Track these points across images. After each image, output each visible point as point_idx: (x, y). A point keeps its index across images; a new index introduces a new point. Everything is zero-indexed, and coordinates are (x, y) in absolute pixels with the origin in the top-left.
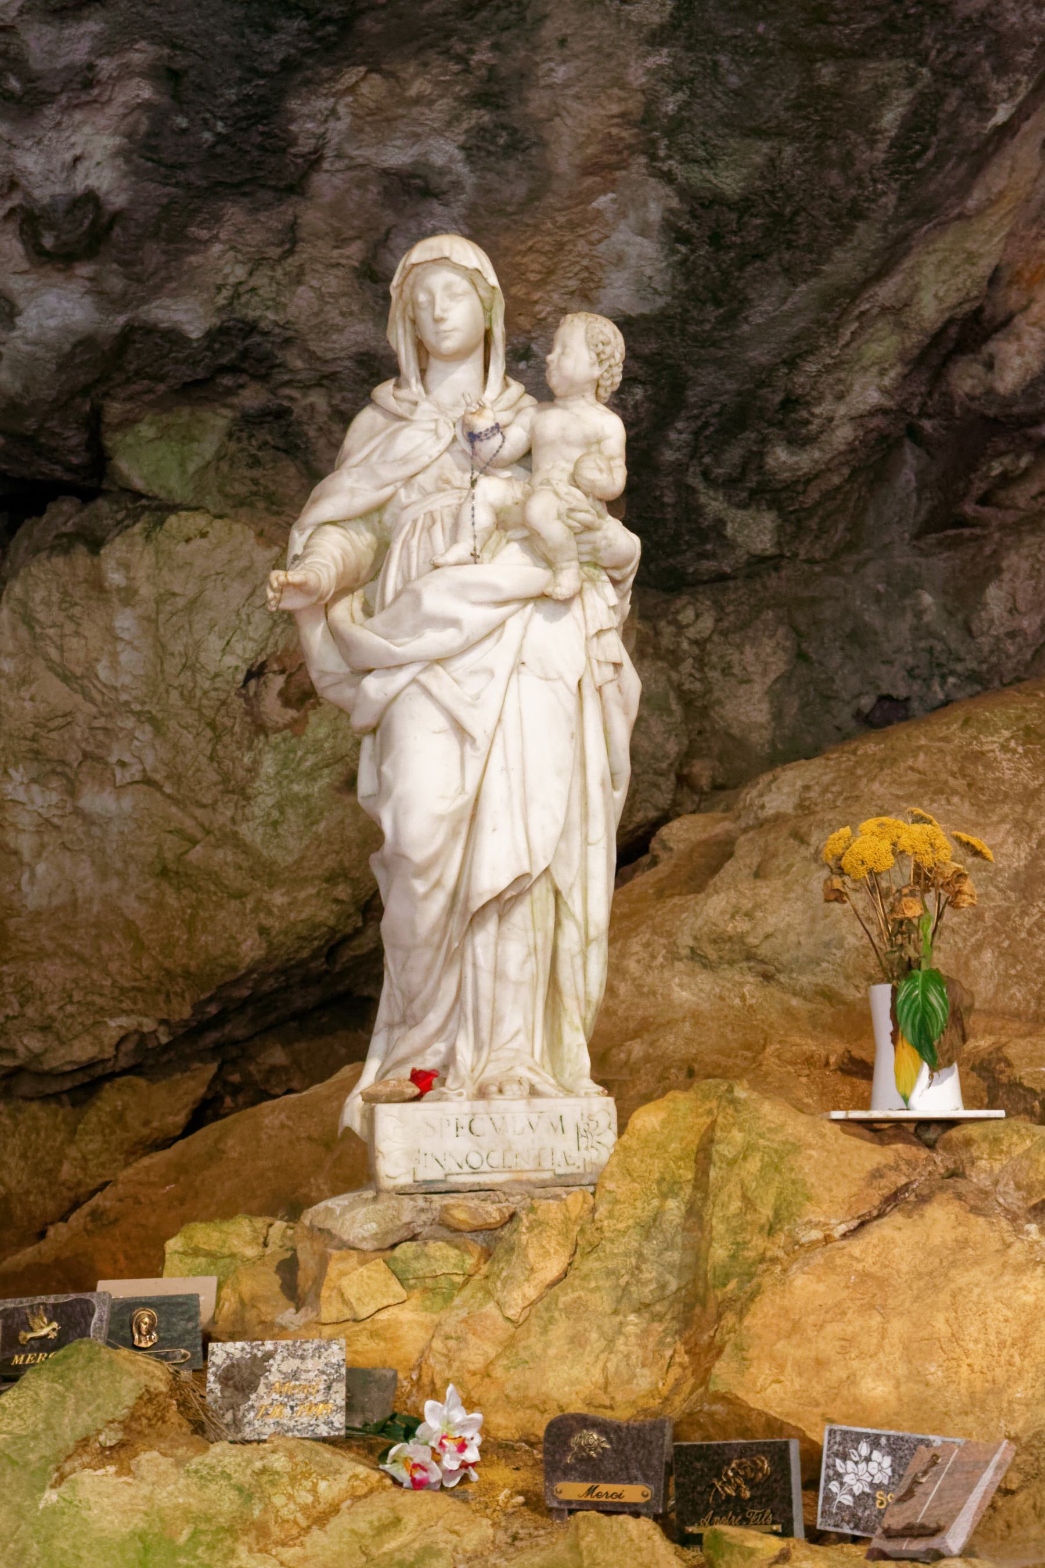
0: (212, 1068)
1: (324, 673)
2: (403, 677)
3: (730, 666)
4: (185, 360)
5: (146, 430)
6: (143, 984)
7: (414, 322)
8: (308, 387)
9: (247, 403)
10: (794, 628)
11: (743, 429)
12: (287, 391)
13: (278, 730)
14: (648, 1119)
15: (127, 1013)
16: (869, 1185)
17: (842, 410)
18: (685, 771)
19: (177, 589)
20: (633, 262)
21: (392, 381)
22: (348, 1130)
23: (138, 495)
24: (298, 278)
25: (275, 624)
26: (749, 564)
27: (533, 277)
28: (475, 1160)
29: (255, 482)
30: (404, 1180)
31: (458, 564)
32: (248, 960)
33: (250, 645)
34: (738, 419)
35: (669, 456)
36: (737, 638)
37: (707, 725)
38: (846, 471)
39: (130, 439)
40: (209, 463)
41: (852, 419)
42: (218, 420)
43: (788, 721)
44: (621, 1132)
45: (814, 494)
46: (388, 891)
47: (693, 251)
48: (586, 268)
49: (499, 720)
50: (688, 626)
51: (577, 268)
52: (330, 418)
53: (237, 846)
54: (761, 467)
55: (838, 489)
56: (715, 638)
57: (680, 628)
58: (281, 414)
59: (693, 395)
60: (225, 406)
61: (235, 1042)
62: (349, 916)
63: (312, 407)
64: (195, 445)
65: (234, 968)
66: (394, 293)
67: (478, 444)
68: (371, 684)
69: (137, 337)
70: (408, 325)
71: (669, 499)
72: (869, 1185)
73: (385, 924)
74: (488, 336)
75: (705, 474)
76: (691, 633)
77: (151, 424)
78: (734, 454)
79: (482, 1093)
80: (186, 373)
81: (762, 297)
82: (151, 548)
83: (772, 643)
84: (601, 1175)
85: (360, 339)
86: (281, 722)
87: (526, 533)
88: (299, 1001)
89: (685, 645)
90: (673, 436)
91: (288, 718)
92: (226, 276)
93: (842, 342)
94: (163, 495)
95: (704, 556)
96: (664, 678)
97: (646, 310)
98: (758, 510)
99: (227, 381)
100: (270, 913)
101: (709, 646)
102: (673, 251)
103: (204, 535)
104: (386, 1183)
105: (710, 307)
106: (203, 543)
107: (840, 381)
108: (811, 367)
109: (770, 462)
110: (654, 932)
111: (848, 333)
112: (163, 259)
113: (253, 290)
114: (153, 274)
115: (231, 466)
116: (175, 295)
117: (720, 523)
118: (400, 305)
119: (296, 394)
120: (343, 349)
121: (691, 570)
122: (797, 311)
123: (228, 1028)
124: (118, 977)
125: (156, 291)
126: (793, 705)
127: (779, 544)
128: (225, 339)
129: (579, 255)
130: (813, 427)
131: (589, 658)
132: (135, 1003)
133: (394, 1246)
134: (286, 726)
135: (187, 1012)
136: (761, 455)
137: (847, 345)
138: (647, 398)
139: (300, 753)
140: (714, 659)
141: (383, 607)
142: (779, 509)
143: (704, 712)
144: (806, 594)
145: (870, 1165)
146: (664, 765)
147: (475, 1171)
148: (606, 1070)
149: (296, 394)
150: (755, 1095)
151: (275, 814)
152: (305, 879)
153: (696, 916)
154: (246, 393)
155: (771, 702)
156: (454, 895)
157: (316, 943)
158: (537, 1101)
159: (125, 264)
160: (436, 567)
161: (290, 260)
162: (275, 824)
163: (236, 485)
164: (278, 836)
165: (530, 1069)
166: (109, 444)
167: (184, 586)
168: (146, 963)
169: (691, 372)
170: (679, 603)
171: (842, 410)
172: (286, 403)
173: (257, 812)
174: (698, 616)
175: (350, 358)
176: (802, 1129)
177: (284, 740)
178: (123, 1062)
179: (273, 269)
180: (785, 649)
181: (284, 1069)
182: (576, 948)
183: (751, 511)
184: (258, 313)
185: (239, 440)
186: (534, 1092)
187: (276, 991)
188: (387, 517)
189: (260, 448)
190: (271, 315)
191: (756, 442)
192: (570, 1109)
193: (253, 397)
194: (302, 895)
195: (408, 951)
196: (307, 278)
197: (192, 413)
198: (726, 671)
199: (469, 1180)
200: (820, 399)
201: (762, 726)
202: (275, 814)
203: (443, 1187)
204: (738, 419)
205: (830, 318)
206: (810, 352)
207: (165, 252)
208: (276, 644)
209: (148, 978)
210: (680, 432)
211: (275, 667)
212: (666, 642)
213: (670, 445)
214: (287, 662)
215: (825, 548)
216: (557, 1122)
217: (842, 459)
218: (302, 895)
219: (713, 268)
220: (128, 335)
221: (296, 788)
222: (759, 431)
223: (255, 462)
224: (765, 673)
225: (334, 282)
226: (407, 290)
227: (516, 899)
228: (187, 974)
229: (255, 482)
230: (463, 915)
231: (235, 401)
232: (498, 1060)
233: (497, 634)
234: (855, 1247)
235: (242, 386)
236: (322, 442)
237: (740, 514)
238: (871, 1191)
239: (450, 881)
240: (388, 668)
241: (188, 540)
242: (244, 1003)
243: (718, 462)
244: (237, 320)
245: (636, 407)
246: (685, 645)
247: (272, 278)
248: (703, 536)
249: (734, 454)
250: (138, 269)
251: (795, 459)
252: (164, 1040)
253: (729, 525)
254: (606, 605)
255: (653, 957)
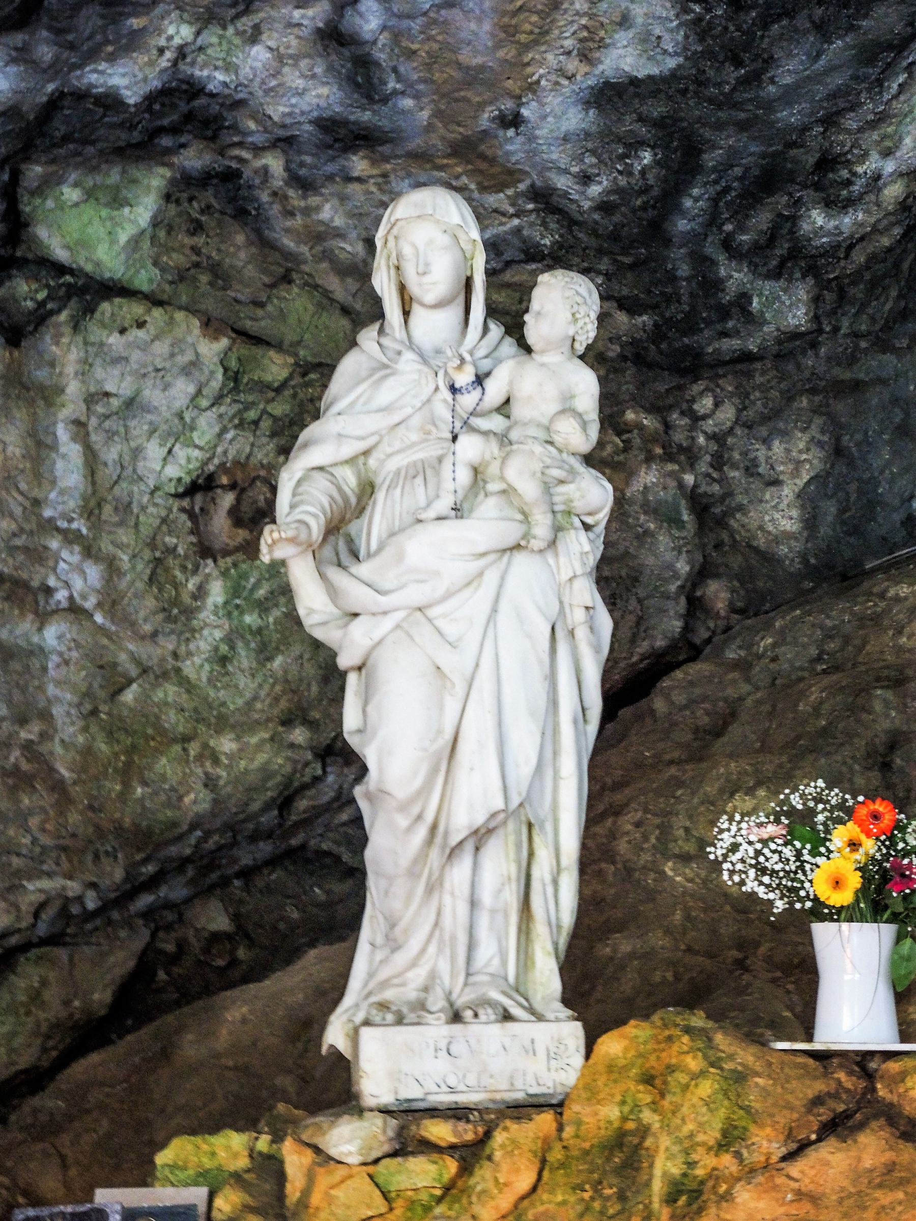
0: (144, 935)
1: (311, 611)
2: (387, 624)
3: (755, 463)
4: (121, 125)
5: (71, 194)
6: (67, 842)
7: (398, 268)
8: (264, 149)
9: (187, 163)
10: (832, 418)
11: (771, 192)
12: (236, 152)
13: (226, 553)
14: (612, 1045)
15: (50, 875)
16: (809, 1111)
17: (889, 167)
18: (698, 593)
19: (110, 387)
20: (640, 20)
21: (377, 326)
22: (333, 1050)
23: (60, 269)
24: (254, 37)
25: (224, 430)
26: (779, 342)
27: (523, 38)
28: (452, 1081)
29: (196, 250)
30: (387, 1099)
31: (440, 518)
32: (191, 814)
33: (196, 453)
34: (768, 180)
35: (682, 225)
36: (763, 431)
37: (725, 536)
38: (897, 231)
39: (50, 203)
40: (143, 232)
41: (901, 175)
42: (155, 180)
43: (824, 531)
44: (588, 1056)
45: (859, 257)
46: (372, 826)
47: (709, 10)
48: (585, 27)
49: (477, 665)
50: (704, 417)
51: (575, 27)
52: (287, 184)
53: (180, 684)
54: (792, 232)
55: (889, 250)
56: (738, 431)
57: (696, 419)
58: (230, 176)
59: (711, 159)
60: (164, 164)
61: (169, 905)
62: (307, 764)
63: (266, 169)
64: (127, 210)
65: (175, 824)
66: (379, 243)
67: (458, 396)
68: (357, 629)
69: (66, 103)
70: (393, 271)
71: (684, 270)
72: (809, 1111)
73: (369, 854)
74: (468, 284)
75: (727, 244)
76: (709, 425)
77: (76, 185)
78: (762, 220)
79: (456, 1017)
80: (123, 137)
81: (790, 55)
82: (79, 339)
83: (806, 437)
84: (567, 1095)
85: (323, 104)
86: (232, 544)
87: (503, 486)
88: (245, 858)
89: (701, 440)
90: (688, 203)
91: (239, 539)
92: (170, 38)
93: (886, 97)
94: (89, 268)
95: (725, 334)
96: (673, 484)
97: (655, 71)
98: (790, 280)
99: (166, 141)
100: (216, 761)
101: (730, 440)
102: (686, 10)
103: (141, 325)
104: (369, 1101)
105: (729, 68)
106: (141, 334)
107: (884, 137)
108: (851, 122)
109: (805, 227)
110: (646, 811)
111: (895, 86)
112: (100, 22)
113: (201, 49)
114: (90, 38)
115: (169, 233)
116: (112, 59)
117: (744, 298)
118: (385, 255)
119: (245, 154)
120: (303, 113)
121: (710, 350)
122: (830, 70)
123: (163, 891)
124: (38, 835)
125: (92, 55)
126: (830, 508)
127: (816, 318)
128: (166, 100)
129: (577, 13)
130: (856, 188)
131: (561, 603)
132: (58, 864)
133: (376, 1161)
134: (237, 549)
135: (119, 874)
136: (794, 219)
137: (896, 97)
138: (657, 163)
139: (252, 580)
140: (736, 456)
141: (369, 555)
142: (815, 277)
143: (721, 522)
144: (847, 375)
145: (811, 1094)
146: (673, 588)
147: (452, 1090)
148: (576, 996)
149: (245, 154)
150: (710, 1024)
151: (224, 649)
152: (257, 722)
153: (693, 793)
154: (190, 152)
155: (803, 507)
156: (434, 828)
157: (269, 794)
158: (510, 1025)
159: (59, 32)
160: (420, 521)
161: (244, 19)
162: (223, 660)
163: (174, 255)
164: (227, 673)
165: (504, 993)
166: (28, 209)
167: (116, 382)
168: (74, 817)
169: (707, 133)
170: (697, 388)
171: (889, 167)
172: (234, 165)
173: (203, 645)
174: (717, 405)
175: (310, 122)
176: (751, 1059)
177: (235, 565)
178: (42, 929)
179: (224, 28)
180: (820, 444)
181: (228, 936)
182: (548, 878)
183: (782, 283)
184: (205, 73)
185: (178, 202)
186: (507, 1017)
187: (220, 848)
188: (372, 462)
189: (202, 212)
190: (220, 76)
191: (787, 206)
192: (541, 1033)
193: (194, 158)
194: (254, 740)
195: (390, 879)
196: (264, 37)
197: (124, 171)
198: (751, 470)
199: (444, 1098)
200: (865, 156)
201: (789, 536)
202: (224, 649)
203: (422, 1105)
204: (768, 180)
205: (873, 72)
206: (852, 109)
207: (102, 17)
208: (225, 453)
209: (74, 835)
210: (696, 200)
211: (225, 480)
212: (679, 437)
213: (683, 213)
214: (239, 476)
215: (873, 320)
216: (528, 1044)
217: (892, 219)
218: (254, 740)
219: (732, 28)
220: (54, 104)
221: (248, 619)
222: (790, 195)
223: (197, 228)
224: (796, 473)
225: (294, 42)
226: (391, 243)
227: (490, 831)
228: (119, 829)
229: (196, 250)
230: (443, 848)
231: (175, 160)
232: (474, 984)
233: (475, 584)
234: (795, 1169)
235: (183, 146)
236: (276, 208)
237: (768, 286)
238: (811, 1118)
239: (429, 817)
240: (374, 614)
241: (123, 331)
242: (185, 861)
243: (741, 228)
244: (182, 81)
245: (643, 172)
246: (701, 440)
247: (221, 37)
248: (724, 313)
249: (762, 220)
250: (70, 37)
251: (833, 223)
252: (91, 905)
253: (755, 301)
254: (581, 551)
255: (646, 838)
